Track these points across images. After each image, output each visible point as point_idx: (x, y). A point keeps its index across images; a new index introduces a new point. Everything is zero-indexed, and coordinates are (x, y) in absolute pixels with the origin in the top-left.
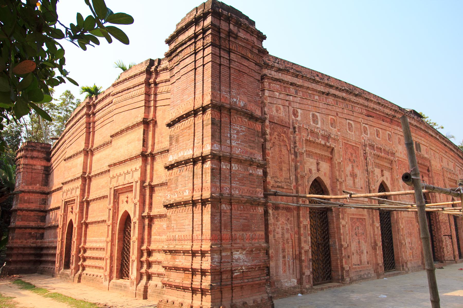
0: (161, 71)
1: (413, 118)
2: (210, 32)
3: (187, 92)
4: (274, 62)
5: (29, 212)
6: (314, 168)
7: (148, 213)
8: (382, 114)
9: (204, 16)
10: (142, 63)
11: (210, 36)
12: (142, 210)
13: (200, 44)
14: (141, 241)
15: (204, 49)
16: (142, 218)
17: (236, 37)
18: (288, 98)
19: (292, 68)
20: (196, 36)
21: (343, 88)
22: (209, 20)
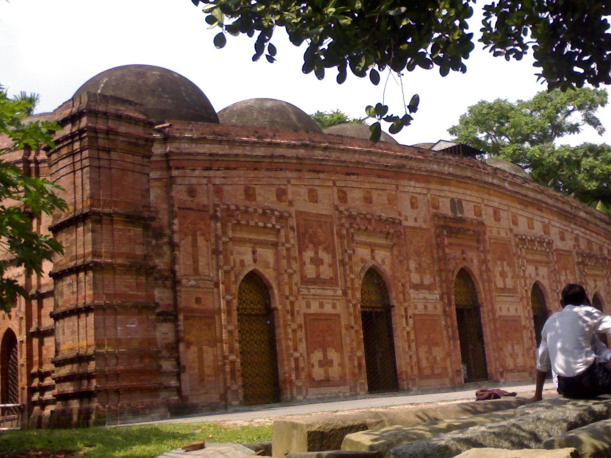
5: (190, 249)
6: (248, 258)
7: (34, 157)
8: (377, 168)
11: (87, 139)
12: (29, 325)
13: (77, 146)
14: (30, 365)
15: (81, 152)
16: (30, 336)
17: (117, 133)
18: (206, 173)
20: (72, 136)
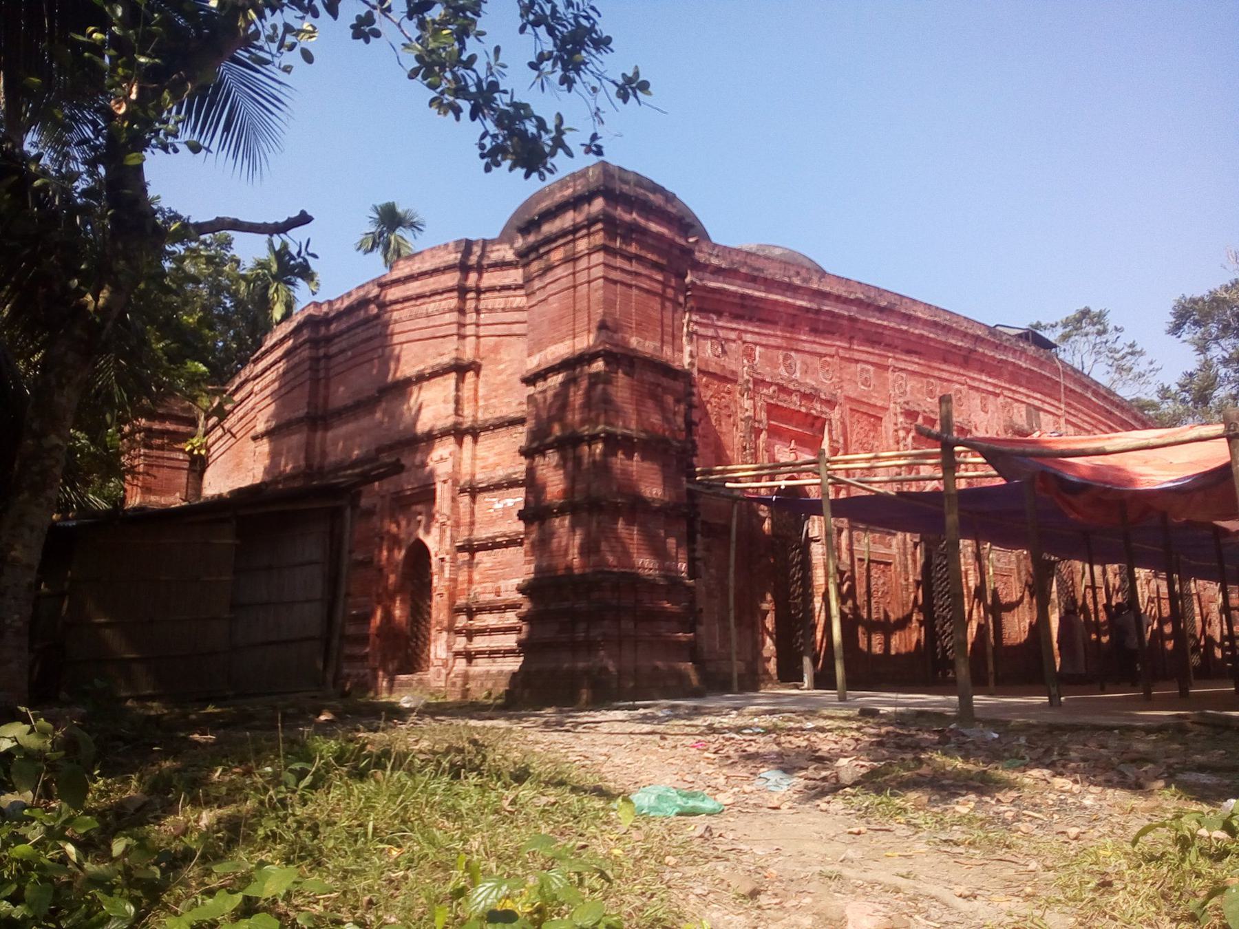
0: (490, 266)
1: (1023, 352)
2: (600, 226)
3: (565, 320)
4: (711, 255)
9: (588, 198)
10: (446, 245)
13: (582, 245)
19: (745, 263)
21: (852, 297)
22: (598, 204)
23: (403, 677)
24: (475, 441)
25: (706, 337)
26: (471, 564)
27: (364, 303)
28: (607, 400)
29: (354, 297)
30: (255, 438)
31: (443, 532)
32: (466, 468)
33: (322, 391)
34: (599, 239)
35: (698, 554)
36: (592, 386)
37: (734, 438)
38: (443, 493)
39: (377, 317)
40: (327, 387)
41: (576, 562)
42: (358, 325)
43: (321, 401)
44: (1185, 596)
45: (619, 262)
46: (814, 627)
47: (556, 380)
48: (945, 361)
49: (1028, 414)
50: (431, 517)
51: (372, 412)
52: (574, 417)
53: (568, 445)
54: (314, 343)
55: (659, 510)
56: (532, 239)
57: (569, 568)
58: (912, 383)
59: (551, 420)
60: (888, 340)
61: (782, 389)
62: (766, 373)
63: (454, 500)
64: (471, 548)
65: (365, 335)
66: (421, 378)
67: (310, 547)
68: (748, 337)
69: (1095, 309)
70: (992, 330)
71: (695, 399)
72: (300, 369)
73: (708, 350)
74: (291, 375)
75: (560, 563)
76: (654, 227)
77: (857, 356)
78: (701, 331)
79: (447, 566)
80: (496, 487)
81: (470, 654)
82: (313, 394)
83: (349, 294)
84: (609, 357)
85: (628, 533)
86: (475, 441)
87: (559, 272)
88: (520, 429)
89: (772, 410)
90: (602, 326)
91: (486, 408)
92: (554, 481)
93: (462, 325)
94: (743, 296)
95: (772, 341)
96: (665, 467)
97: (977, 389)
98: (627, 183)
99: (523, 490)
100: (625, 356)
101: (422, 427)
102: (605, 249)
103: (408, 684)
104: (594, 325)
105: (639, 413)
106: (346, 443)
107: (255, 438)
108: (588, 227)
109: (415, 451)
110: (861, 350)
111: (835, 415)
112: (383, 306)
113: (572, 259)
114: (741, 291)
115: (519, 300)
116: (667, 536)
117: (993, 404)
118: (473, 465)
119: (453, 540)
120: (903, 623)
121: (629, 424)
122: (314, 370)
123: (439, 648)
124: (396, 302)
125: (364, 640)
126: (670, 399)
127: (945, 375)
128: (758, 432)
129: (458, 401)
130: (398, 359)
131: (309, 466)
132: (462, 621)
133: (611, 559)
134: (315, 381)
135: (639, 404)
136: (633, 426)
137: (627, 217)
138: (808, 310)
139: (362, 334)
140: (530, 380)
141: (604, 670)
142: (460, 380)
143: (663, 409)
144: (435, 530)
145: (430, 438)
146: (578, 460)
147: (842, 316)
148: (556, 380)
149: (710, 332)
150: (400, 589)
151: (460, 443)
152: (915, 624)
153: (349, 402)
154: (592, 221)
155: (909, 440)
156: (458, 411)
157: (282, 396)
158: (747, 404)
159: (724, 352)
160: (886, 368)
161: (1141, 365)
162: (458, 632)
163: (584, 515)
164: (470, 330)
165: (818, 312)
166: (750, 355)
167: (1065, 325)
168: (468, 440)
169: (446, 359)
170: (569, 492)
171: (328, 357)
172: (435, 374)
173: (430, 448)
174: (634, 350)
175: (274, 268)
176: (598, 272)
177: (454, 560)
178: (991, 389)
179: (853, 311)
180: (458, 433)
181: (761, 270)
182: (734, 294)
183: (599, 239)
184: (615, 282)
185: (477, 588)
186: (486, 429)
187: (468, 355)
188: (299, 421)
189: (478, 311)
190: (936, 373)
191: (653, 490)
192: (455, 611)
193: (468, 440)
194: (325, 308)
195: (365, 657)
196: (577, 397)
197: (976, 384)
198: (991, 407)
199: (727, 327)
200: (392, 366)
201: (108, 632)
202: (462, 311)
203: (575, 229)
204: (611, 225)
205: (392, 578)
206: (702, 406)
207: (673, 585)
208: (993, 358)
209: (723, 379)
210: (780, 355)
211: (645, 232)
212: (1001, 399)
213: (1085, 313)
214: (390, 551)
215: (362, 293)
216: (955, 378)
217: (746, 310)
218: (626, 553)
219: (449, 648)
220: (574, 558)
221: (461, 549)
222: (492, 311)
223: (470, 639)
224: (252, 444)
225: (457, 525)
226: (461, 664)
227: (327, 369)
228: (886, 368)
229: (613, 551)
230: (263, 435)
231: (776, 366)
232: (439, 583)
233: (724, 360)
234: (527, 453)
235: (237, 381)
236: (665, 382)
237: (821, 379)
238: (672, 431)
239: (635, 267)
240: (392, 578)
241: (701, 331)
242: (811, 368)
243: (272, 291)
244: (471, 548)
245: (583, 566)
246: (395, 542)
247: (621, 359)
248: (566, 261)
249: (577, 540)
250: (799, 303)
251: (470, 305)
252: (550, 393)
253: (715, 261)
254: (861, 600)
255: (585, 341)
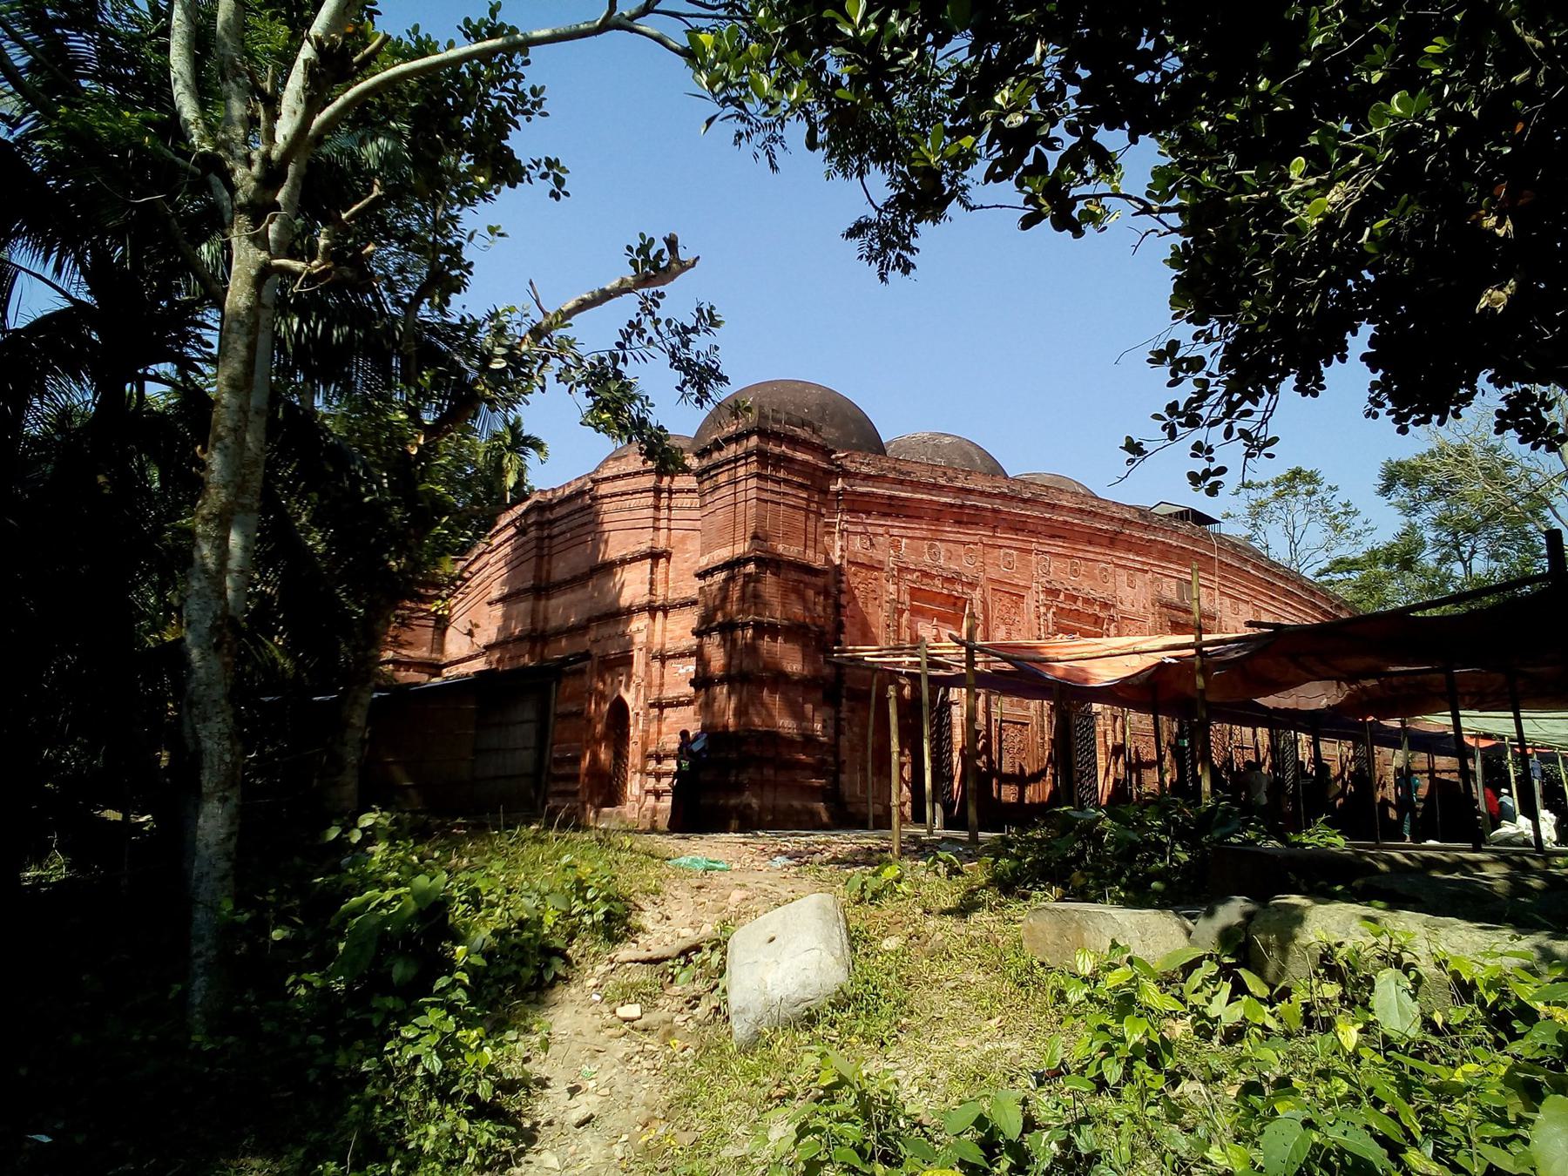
9: (746, 435)
13: (741, 471)
23: (606, 810)
24: (666, 616)
25: (856, 533)
26: (660, 719)
27: (580, 493)
28: (756, 596)
29: (573, 488)
30: (490, 604)
31: (638, 691)
32: (657, 639)
33: (546, 567)
34: (753, 468)
35: (843, 715)
36: (745, 584)
37: (879, 617)
38: (639, 658)
39: (590, 506)
40: (549, 562)
41: (731, 721)
42: (576, 512)
43: (544, 575)
44: (1370, 760)
45: (770, 485)
46: (952, 778)
47: (720, 577)
48: (1090, 543)
49: (1179, 587)
50: (630, 677)
51: (584, 586)
52: (733, 607)
53: (728, 628)
54: (540, 525)
55: (797, 683)
56: (705, 462)
57: (726, 726)
58: (1056, 564)
59: (716, 609)
60: (1031, 527)
61: (925, 574)
62: (910, 560)
63: (647, 664)
64: (660, 705)
65: (580, 521)
66: (624, 562)
67: (528, 712)
68: (895, 531)
69: (1307, 469)
70: (1143, 513)
71: (844, 586)
72: (528, 547)
73: (857, 543)
74: (520, 551)
75: (719, 721)
76: (799, 456)
77: (1000, 542)
78: (851, 528)
79: (641, 719)
80: (682, 655)
81: (644, 794)
82: (538, 567)
83: (569, 484)
84: (759, 562)
85: (774, 701)
86: (666, 616)
87: (724, 492)
88: (695, 609)
89: (915, 593)
90: (755, 537)
91: (675, 589)
92: (717, 659)
93: (657, 519)
94: (890, 497)
95: (918, 534)
96: (805, 647)
97: (1124, 567)
98: (779, 422)
99: (694, 659)
100: (771, 560)
101: (624, 601)
102: (759, 476)
103: (609, 815)
104: (749, 535)
105: (784, 605)
106: (563, 609)
107: (490, 604)
108: (746, 458)
109: (619, 622)
110: (1003, 538)
111: (977, 595)
112: (594, 499)
113: (734, 482)
114: (888, 493)
115: (697, 514)
116: (805, 701)
117: (1139, 579)
118: (663, 635)
119: (646, 699)
120: (1037, 777)
121: (775, 614)
122: (539, 547)
123: (633, 787)
124: (605, 497)
125: (575, 778)
126: (811, 593)
127: (1090, 556)
128: (901, 612)
129: (652, 583)
130: (606, 542)
131: (534, 630)
132: (652, 765)
133: (757, 720)
134: (540, 557)
135: (785, 596)
136: (778, 615)
137: (777, 450)
138: (952, 505)
139: (578, 519)
140: (702, 575)
141: (749, 805)
142: (654, 565)
143: (802, 598)
144: (633, 690)
145: (630, 612)
146: (734, 641)
147: (986, 509)
148: (720, 577)
149: (860, 529)
150: (605, 737)
151: (653, 617)
152: (1049, 777)
153: (568, 577)
154: (748, 454)
155: (1050, 615)
156: (651, 592)
157: (514, 564)
158: (892, 588)
159: (872, 545)
160: (1029, 552)
161: (1357, 524)
162: (649, 774)
163: (737, 685)
164: (663, 524)
165: (962, 506)
166: (897, 547)
167: (1277, 485)
168: (660, 615)
169: (644, 548)
170: (727, 666)
171: (551, 537)
172: (634, 560)
173: (628, 622)
174: (780, 555)
175: (509, 440)
176: (752, 493)
177: (647, 714)
178: (1138, 566)
179: (998, 504)
180: (651, 609)
181: (909, 473)
182: (882, 496)
183: (753, 468)
184: (766, 501)
185: (664, 738)
186: (674, 607)
187: (661, 545)
188: (526, 590)
189: (669, 508)
190: (1080, 554)
191: (794, 665)
192: (647, 757)
193: (660, 615)
194: (549, 495)
195: (576, 793)
196: (735, 593)
197: (1123, 562)
198: (1138, 583)
199: (876, 525)
200: (602, 547)
201: (394, 768)
202: (657, 508)
203: (736, 459)
204: (763, 456)
205: (599, 728)
206: (851, 591)
207: (809, 741)
208: (1141, 539)
209: (872, 568)
210: (926, 544)
211: (792, 460)
212: (1149, 575)
213: (1297, 473)
214: (597, 704)
215: (579, 484)
216: (1100, 557)
217: (893, 509)
218: (771, 716)
219: (642, 787)
220: (730, 719)
221: (652, 706)
222: (681, 508)
223: (658, 780)
224: (488, 608)
225: (650, 685)
226: (651, 799)
227: (550, 547)
228: (1029, 552)
229: (759, 714)
230: (498, 601)
231: (922, 554)
232: (635, 733)
233: (871, 552)
234: (698, 633)
235: (476, 552)
236: (806, 578)
237: (964, 564)
238: (813, 618)
239: (784, 488)
240: (599, 728)
241: (851, 528)
242: (953, 554)
243: (506, 460)
244: (660, 705)
245: (737, 724)
246: (602, 696)
247: (770, 563)
248: (729, 483)
249: (732, 705)
250: (943, 500)
251: (664, 502)
252: (715, 587)
253: (864, 469)
254: (995, 756)
255: (741, 548)
